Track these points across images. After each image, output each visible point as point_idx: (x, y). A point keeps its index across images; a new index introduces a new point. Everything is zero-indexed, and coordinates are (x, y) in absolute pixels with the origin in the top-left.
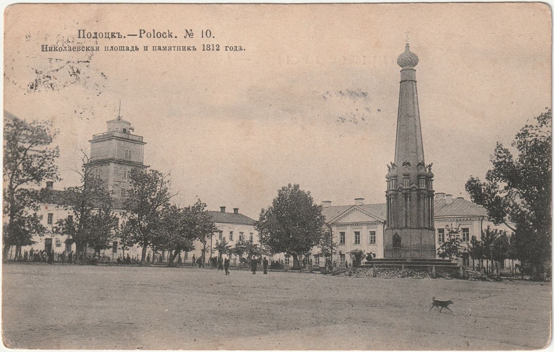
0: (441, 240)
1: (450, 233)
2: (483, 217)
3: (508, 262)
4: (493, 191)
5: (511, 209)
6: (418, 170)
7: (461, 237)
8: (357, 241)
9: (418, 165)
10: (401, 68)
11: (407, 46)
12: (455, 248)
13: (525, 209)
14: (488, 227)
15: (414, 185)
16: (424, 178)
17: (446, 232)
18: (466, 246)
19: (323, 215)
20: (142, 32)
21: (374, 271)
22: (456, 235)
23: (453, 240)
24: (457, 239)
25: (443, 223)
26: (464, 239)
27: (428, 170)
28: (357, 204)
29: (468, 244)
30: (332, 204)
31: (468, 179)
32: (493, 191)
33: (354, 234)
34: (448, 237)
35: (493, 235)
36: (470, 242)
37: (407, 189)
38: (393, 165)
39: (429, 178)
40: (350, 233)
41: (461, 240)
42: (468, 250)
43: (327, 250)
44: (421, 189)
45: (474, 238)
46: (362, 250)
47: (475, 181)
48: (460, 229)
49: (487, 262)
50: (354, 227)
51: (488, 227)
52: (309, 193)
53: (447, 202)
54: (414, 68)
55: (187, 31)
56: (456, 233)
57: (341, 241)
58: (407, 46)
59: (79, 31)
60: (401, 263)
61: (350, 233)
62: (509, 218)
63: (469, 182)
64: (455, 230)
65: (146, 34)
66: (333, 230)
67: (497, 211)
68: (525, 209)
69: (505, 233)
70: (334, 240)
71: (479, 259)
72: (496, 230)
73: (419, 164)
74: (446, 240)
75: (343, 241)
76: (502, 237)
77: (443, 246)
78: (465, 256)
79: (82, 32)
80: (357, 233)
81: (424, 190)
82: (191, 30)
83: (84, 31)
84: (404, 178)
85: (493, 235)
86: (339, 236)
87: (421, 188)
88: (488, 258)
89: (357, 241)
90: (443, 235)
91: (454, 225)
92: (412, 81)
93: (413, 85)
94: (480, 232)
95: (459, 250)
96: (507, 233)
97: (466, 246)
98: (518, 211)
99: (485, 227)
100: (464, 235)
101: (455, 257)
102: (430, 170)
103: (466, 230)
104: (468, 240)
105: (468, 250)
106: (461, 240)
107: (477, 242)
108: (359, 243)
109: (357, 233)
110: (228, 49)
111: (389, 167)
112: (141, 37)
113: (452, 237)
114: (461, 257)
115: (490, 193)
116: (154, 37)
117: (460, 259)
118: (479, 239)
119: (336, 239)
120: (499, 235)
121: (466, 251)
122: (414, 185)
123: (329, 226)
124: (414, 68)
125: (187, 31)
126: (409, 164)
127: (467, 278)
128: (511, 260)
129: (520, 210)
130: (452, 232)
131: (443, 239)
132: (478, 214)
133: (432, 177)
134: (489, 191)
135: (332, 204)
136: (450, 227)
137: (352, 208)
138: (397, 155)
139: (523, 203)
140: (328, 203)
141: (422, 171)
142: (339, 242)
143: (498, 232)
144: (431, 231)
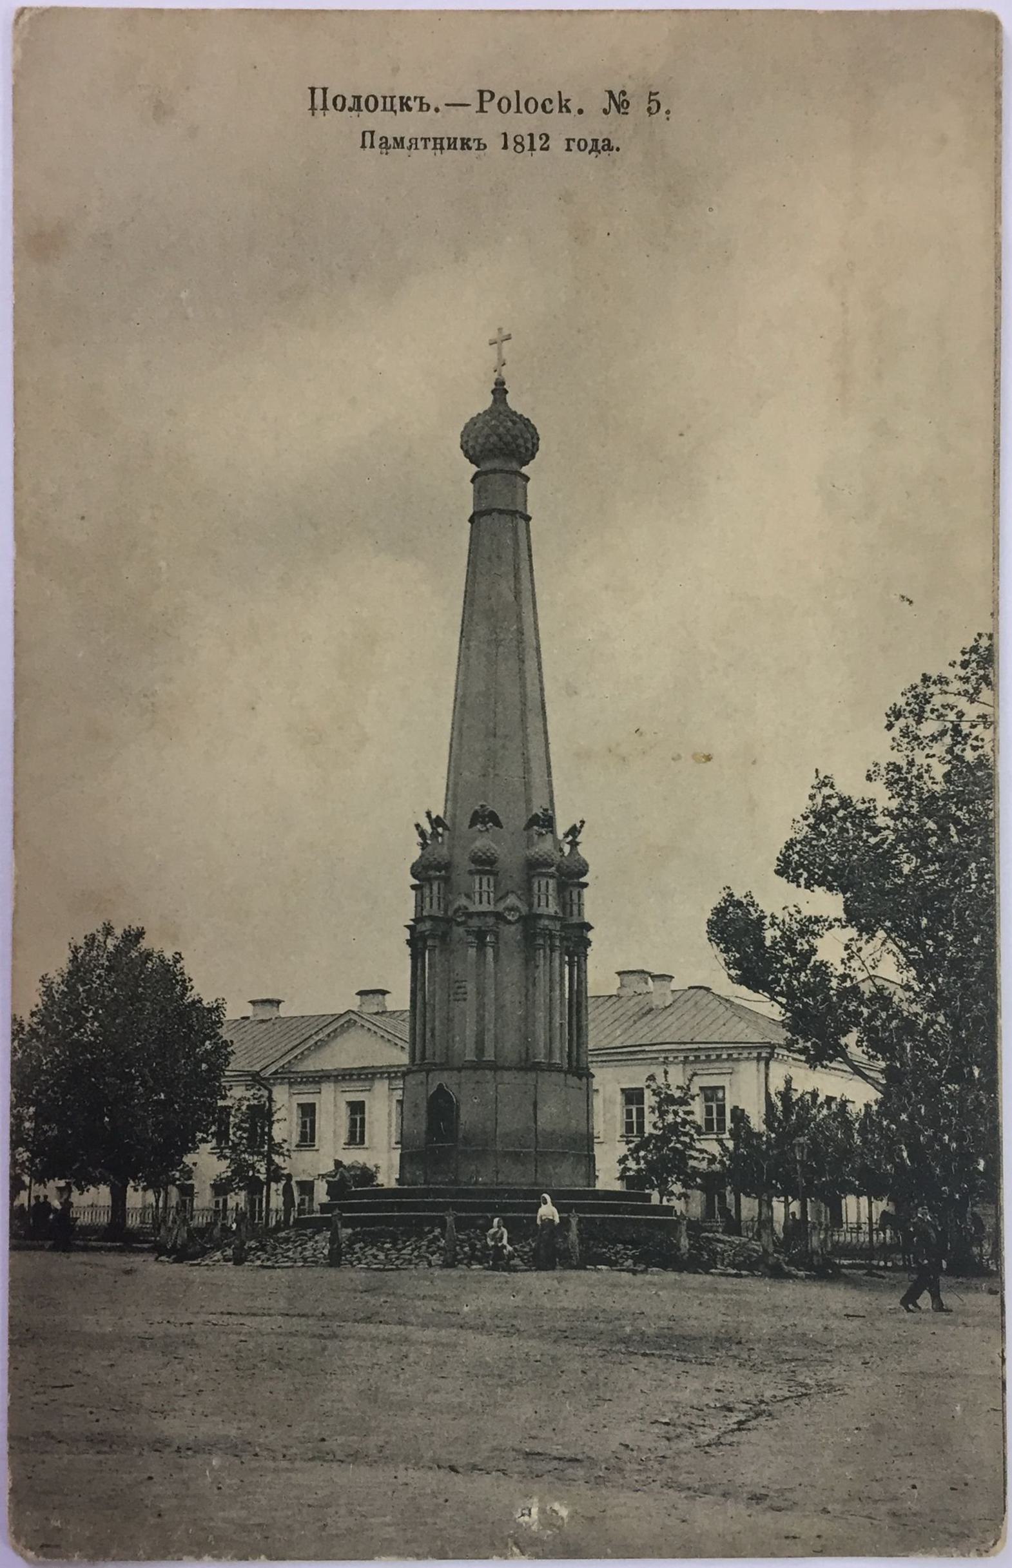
0: (633, 1127)
1: (660, 1104)
2: (773, 1047)
3: (855, 1208)
4: (802, 945)
5: (866, 1012)
6: (530, 843)
7: (699, 1117)
8: (356, 1137)
9: (529, 826)
10: (474, 469)
11: (500, 390)
12: (681, 1157)
13: (916, 1008)
14: (788, 1081)
15: (511, 900)
16: (552, 876)
17: (650, 1100)
18: (714, 1148)
19: (226, 1037)
20: (487, 96)
21: (334, 1239)
22: (681, 1110)
23: (673, 1129)
24: (685, 1122)
25: (642, 1068)
26: (709, 1123)
27: (567, 849)
28: (365, 1009)
29: (720, 1142)
30: (284, 1011)
31: (715, 900)
32: (802, 945)
33: (344, 1111)
34: (655, 1117)
35: (806, 1108)
36: (727, 1135)
37: (484, 914)
38: (436, 822)
39: (572, 877)
40: (331, 1106)
41: (698, 1130)
42: (722, 1162)
43: (252, 1166)
44: (540, 916)
45: (739, 1116)
46: (370, 1165)
47: (739, 904)
48: (695, 1090)
49: (787, 1205)
50: (345, 1086)
51: (788, 1081)
52: (178, 958)
53: (657, 1002)
54: (524, 470)
55: (611, 93)
56: (683, 1102)
57: (303, 1136)
58: (500, 390)
59: (313, 90)
60: (444, 1207)
61: (331, 1106)
62: (859, 1043)
63: (720, 911)
64: (678, 1094)
65: (496, 100)
66: (275, 1096)
67: (819, 1020)
68: (916, 1008)
69: (844, 1104)
70: (279, 1132)
71: (759, 1197)
72: (815, 1095)
73: (534, 821)
74: (648, 1129)
75: (308, 1138)
76: (833, 1117)
77: (637, 1149)
78: (711, 1184)
79: (368, 135)
80: (357, 1108)
81: (550, 917)
82: (623, 93)
83: (372, 133)
84: (471, 873)
85: (806, 1108)
86: (295, 1117)
87: (540, 911)
88: (790, 1191)
89: (356, 1137)
90: (641, 1113)
91: (677, 1077)
92: (513, 513)
93: (515, 530)
94: (763, 1095)
95: (692, 1163)
96: (850, 1107)
97: (714, 1148)
98: (890, 1018)
99: (777, 1084)
100: (709, 1111)
101: (677, 1188)
102: (574, 844)
103: (710, 1093)
104: (722, 1129)
105: (722, 1162)
106: (698, 1130)
107: (749, 1131)
108: (362, 1141)
109: (357, 1108)
110: (574, 146)
111: (422, 834)
112: (482, 110)
113: (670, 1118)
114: (698, 1187)
115: (793, 953)
116: (518, 111)
117: (697, 1194)
118: (757, 1123)
119: (285, 1129)
120: (825, 1112)
121: (717, 1167)
122: (511, 900)
123: (256, 1079)
124: (524, 470)
125: (611, 93)
126: (494, 818)
127: (706, 1269)
128: (864, 1200)
129: (898, 1014)
130: (671, 1100)
131: (641, 1126)
132: (756, 1038)
133: (584, 874)
134: (790, 948)
135: (284, 1011)
136: (660, 1080)
137: (345, 1023)
138: (453, 794)
139: (907, 988)
140: (268, 1007)
141: (545, 846)
142: (296, 1139)
143: (821, 1099)
144: (573, 1080)
